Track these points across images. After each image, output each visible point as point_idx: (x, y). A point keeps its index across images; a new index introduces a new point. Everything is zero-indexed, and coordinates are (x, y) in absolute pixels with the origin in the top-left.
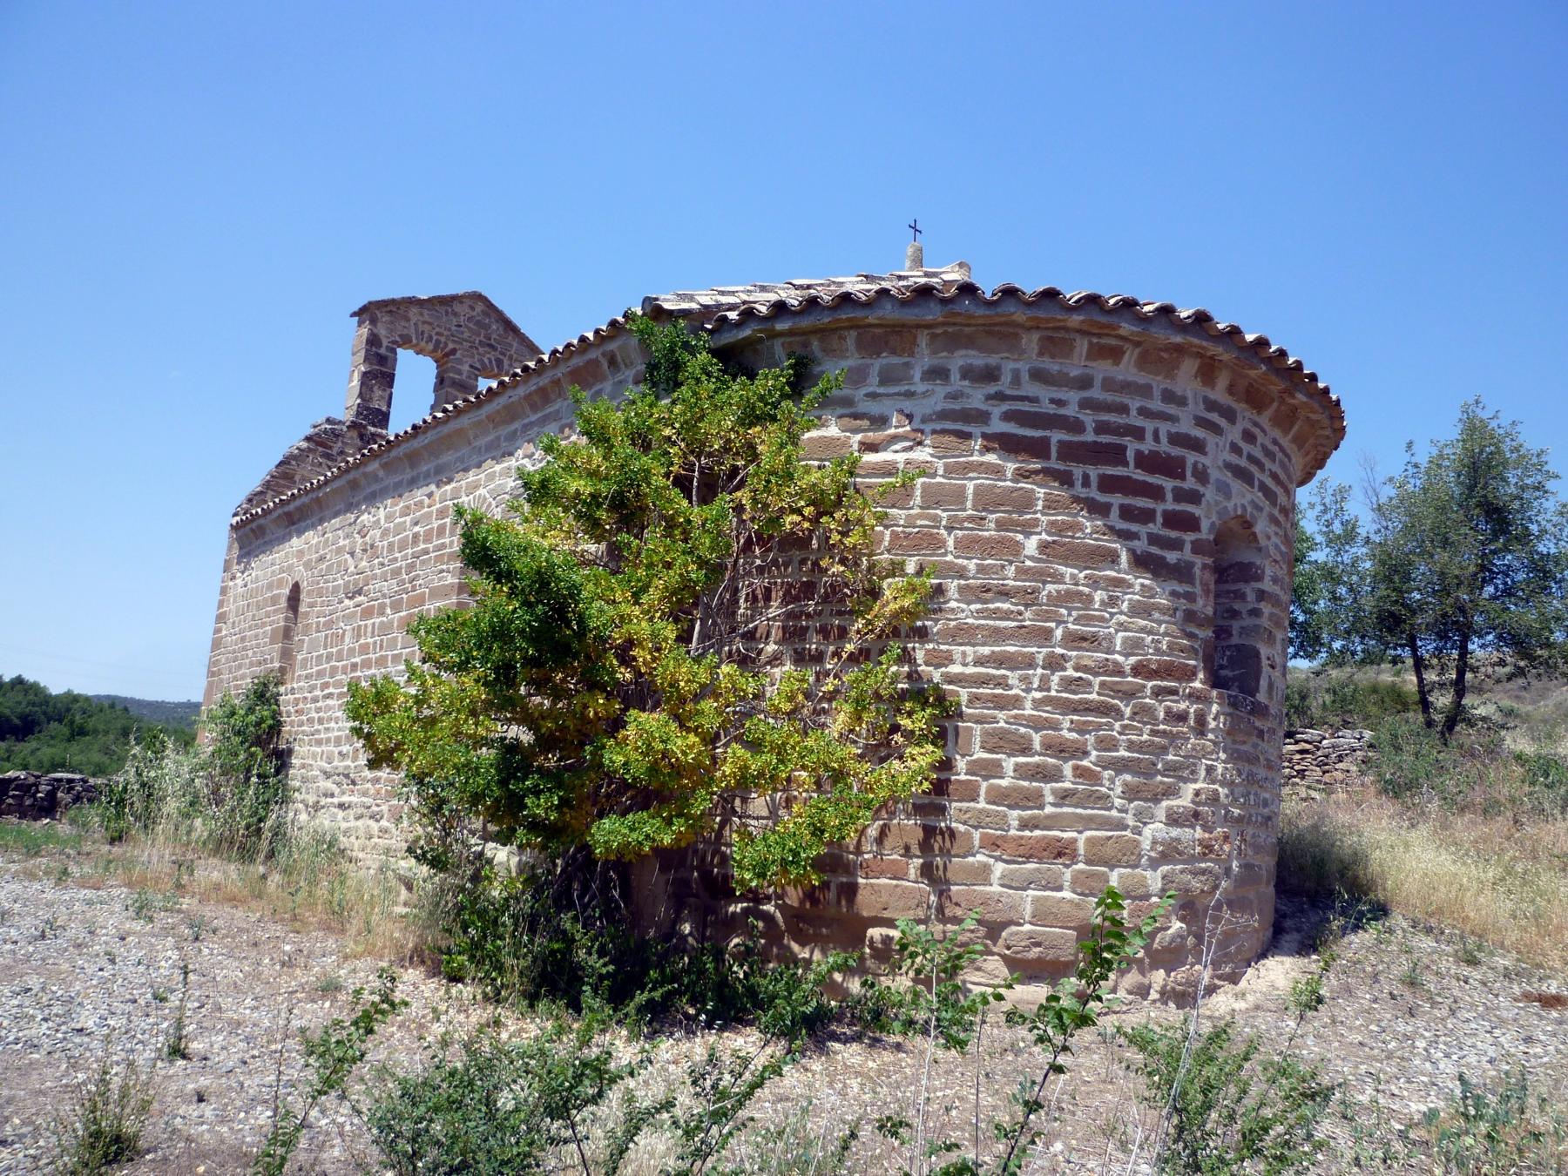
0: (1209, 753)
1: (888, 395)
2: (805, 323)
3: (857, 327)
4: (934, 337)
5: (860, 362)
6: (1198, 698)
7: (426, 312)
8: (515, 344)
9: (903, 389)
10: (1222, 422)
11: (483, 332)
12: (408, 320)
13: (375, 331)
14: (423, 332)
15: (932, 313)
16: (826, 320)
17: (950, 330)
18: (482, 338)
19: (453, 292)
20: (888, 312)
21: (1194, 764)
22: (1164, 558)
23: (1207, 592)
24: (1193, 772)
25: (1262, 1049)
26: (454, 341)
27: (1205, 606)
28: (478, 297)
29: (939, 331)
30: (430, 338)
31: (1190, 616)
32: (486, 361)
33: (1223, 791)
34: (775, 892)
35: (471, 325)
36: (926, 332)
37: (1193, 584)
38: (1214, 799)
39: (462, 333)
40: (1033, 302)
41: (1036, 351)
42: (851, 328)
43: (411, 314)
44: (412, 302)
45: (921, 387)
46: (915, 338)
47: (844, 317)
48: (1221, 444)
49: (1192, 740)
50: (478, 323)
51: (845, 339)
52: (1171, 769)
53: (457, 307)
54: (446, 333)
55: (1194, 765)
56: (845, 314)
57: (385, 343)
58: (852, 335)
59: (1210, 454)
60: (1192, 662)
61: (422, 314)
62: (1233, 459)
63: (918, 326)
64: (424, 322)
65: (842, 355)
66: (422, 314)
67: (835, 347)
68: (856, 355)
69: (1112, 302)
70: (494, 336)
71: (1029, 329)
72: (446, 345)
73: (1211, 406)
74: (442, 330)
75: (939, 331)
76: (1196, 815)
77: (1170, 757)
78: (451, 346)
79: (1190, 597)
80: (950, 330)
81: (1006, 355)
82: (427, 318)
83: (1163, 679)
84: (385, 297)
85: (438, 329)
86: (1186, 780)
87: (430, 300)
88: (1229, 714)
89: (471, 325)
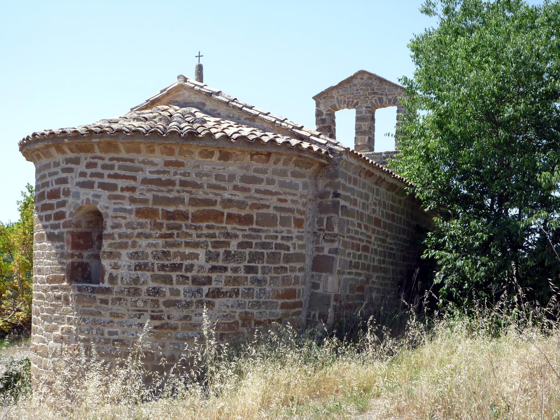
0: (69, 312)
6: (65, 289)
7: (340, 91)
8: (387, 87)
10: (73, 166)
11: (369, 88)
12: (333, 97)
13: (319, 109)
14: (341, 100)
18: (370, 91)
19: (349, 76)
21: (63, 317)
22: (54, 233)
23: (68, 243)
24: (63, 320)
26: (356, 99)
27: (67, 249)
28: (362, 73)
30: (345, 101)
31: (62, 255)
32: (374, 101)
33: (74, 327)
35: (363, 87)
37: (63, 241)
38: (69, 331)
39: (360, 93)
43: (334, 95)
44: (332, 89)
48: (74, 176)
49: (64, 307)
50: (366, 85)
52: (56, 319)
53: (355, 82)
54: (351, 96)
55: (63, 317)
57: (325, 112)
59: (70, 183)
60: (62, 275)
61: (338, 92)
62: (82, 179)
64: (340, 96)
66: (338, 92)
70: (375, 87)
72: (353, 101)
73: (68, 161)
74: (349, 96)
76: (62, 338)
77: (56, 315)
78: (355, 101)
79: (62, 247)
82: (341, 93)
83: (54, 283)
84: (323, 89)
85: (347, 96)
86: (61, 324)
87: (341, 84)
88: (77, 295)
89: (363, 87)
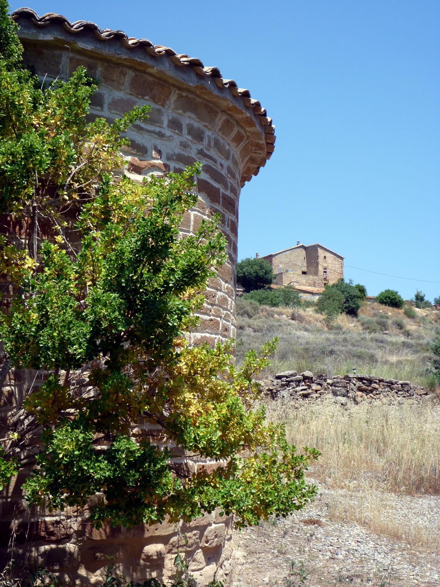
1: (148, 131)
2: (107, 51)
3: (135, 70)
4: (180, 97)
5: (129, 97)
9: (158, 129)
15: (192, 82)
16: (124, 57)
17: (190, 96)
20: (166, 68)
25: (346, 445)
29: (184, 94)
34: (198, 362)
36: (177, 92)
40: (133, 48)
41: (219, 127)
42: (130, 68)
45: (168, 132)
46: (170, 93)
47: (139, 60)
51: (125, 75)
56: (139, 58)
58: (131, 74)
63: (174, 86)
65: (118, 87)
67: (115, 78)
68: (128, 91)
69: (130, 42)
71: (223, 111)
75: (184, 94)
80: (190, 96)
81: (207, 124)
